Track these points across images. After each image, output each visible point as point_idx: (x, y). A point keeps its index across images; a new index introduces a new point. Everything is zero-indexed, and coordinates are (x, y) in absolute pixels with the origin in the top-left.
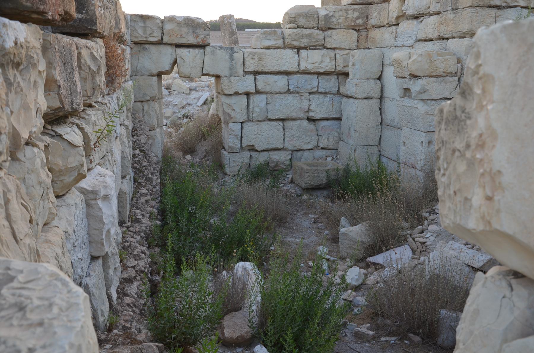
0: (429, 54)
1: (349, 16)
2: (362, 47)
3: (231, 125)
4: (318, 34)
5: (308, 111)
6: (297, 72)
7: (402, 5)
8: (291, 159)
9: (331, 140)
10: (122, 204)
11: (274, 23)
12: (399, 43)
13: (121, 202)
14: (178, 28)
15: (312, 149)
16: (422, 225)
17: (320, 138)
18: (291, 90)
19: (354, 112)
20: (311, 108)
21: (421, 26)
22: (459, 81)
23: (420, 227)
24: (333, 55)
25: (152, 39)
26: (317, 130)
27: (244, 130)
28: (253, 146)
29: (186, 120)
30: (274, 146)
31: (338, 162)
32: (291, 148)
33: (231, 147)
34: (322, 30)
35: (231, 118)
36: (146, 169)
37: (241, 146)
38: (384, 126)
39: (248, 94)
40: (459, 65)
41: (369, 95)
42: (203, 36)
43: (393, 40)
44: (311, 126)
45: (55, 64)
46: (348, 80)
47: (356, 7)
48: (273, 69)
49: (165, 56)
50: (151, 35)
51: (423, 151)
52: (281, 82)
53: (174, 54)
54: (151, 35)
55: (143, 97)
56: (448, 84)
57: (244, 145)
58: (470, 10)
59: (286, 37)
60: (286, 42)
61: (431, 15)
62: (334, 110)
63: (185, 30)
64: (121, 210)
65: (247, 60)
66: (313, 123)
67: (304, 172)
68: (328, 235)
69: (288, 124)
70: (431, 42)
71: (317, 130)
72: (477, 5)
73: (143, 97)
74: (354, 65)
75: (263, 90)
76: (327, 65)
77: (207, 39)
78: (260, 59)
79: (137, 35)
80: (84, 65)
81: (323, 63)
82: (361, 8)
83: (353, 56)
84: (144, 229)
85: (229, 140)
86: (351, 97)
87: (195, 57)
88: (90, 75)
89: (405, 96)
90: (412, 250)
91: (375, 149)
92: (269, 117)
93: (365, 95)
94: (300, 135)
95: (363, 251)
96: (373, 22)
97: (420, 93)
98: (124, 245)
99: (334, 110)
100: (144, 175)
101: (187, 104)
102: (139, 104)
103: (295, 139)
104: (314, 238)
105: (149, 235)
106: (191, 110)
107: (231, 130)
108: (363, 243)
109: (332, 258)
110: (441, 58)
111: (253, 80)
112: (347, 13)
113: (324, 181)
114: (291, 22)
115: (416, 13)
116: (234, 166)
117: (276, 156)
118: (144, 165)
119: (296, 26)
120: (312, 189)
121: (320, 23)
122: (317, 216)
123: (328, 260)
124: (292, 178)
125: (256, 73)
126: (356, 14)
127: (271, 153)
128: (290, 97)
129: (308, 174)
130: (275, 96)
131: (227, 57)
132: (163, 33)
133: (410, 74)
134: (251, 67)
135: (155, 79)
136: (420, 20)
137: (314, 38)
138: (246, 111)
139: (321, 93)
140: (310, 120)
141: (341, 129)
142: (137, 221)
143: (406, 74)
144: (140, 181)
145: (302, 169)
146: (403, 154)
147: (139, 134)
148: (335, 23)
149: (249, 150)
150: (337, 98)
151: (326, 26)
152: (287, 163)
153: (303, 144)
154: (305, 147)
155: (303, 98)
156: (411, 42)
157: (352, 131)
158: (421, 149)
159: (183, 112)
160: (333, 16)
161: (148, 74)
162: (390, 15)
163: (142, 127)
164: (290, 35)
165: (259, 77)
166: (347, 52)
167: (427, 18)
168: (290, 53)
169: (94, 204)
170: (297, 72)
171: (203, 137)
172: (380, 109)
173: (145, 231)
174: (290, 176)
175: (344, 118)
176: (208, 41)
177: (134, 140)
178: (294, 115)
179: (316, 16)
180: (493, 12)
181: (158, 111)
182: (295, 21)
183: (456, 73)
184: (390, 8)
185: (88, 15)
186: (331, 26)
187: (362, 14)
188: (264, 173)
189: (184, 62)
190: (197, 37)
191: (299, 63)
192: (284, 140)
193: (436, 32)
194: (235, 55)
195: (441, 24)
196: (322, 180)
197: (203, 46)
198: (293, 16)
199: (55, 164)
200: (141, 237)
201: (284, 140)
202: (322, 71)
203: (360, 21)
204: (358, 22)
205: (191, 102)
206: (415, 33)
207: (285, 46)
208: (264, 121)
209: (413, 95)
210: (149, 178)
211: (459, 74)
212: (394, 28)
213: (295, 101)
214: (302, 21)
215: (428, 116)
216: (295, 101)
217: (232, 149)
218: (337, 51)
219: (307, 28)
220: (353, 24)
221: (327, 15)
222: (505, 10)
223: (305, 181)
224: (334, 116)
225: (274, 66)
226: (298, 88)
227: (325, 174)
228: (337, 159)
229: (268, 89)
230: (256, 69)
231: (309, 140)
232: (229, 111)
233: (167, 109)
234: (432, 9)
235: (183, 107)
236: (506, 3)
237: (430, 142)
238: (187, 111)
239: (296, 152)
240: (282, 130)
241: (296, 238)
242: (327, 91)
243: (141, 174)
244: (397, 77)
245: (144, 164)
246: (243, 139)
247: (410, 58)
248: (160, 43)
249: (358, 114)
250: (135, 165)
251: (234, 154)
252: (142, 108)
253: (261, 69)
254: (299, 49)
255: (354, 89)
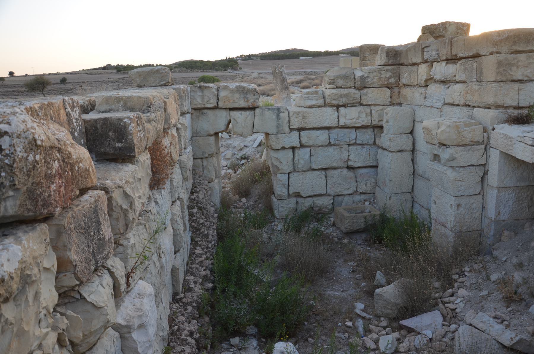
0: (457, 126)
1: (382, 76)
2: (395, 102)
3: (279, 176)
4: (354, 94)
5: (347, 161)
6: (337, 127)
7: (430, 70)
8: (333, 203)
9: (368, 185)
10: (175, 278)
11: (323, 51)
12: (428, 103)
13: (174, 276)
14: (231, 95)
15: (352, 194)
16: (452, 288)
17: (358, 183)
18: (332, 143)
19: (389, 163)
20: (350, 158)
21: (448, 91)
22: (485, 149)
23: (450, 290)
24: (369, 111)
25: (209, 106)
26: (356, 177)
27: (290, 180)
28: (299, 193)
29: (243, 161)
30: (317, 193)
31: (375, 206)
32: (332, 193)
33: (280, 195)
34: (358, 89)
35: (279, 170)
36: (203, 226)
37: (288, 193)
38: (416, 175)
39: (293, 148)
40: (486, 134)
41: (402, 148)
42: (252, 100)
43: (423, 100)
44: (351, 174)
45: (69, 246)
46: (383, 134)
47: (389, 67)
48: (315, 126)
49: (222, 117)
50: (208, 102)
51: (453, 213)
52: (322, 137)
53: (228, 116)
54: (208, 102)
55: (203, 155)
56: (475, 152)
57: (291, 193)
58: (494, 84)
59: (327, 97)
60: (327, 101)
61: (458, 82)
62: (371, 159)
63: (237, 95)
64: (174, 283)
65: (292, 118)
66: (352, 170)
67: (345, 218)
68: (364, 286)
69: (330, 173)
70: (458, 107)
71: (356, 177)
72: (500, 80)
73: (203, 155)
74: (387, 122)
75: (307, 144)
76: (364, 120)
77: (257, 102)
78: (304, 117)
79: (196, 103)
80: (115, 207)
81: (360, 119)
82: (393, 69)
83: (387, 114)
84: (195, 298)
85: (278, 189)
86: (386, 149)
87: (247, 118)
88: (122, 214)
89: (434, 160)
90: (443, 315)
91: (409, 196)
92: (313, 168)
93: (398, 149)
94: (341, 183)
95: (396, 312)
96: (404, 81)
97: (448, 160)
98: (173, 330)
99: (371, 159)
100: (201, 233)
101: (245, 146)
102: (199, 160)
103: (336, 186)
104: (351, 291)
105: (200, 304)
106: (247, 152)
107: (279, 180)
108: (396, 304)
109: (368, 316)
110: (467, 128)
111: (298, 135)
112: (380, 73)
113: (363, 226)
114: (330, 84)
115: (443, 79)
116: (282, 211)
117: (320, 202)
118: (201, 222)
119: (335, 87)
120: (350, 234)
121: (356, 83)
122: (355, 264)
123: (364, 318)
124: (334, 222)
125: (300, 130)
126: (389, 74)
127: (315, 199)
128: (331, 150)
129: (348, 221)
130: (317, 148)
131: (274, 117)
132: (218, 99)
133: (439, 143)
134: (296, 124)
135: (212, 138)
136: (447, 86)
137: (351, 97)
138: (292, 163)
139: (359, 144)
140: (349, 168)
141: (377, 175)
142: (190, 290)
143: (436, 142)
144: (196, 239)
145: (343, 215)
146: (434, 212)
147: (198, 190)
148: (370, 83)
149: (296, 196)
150: (374, 149)
151: (362, 85)
152: (330, 207)
153: (343, 189)
154: (346, 192)
155: (343, 150)
156: (439, 104)
157: (388, 181)
158: (451, 211)
159: (241, 153)
160: (368, 77)
161: (206, 134)
162: (420, 77)
163: (202, 182)
164: (329, 95)
165: (303, 133)
166: (381, 107)
167: (453, 85)
168: (330, 111)
169: (129, 337)
170: (337, 127)
171: (255, 182)
172: (412, 160)
173: (196, 300)
174: (332, 219)
175: (380, 166)
176: (258, 104)
177: (193, 197)
178: (335, 165)
179: (352, 77)
180: (516, 86)
181: (216, 165)
182: (334, 83)
183: (483, 141)
184: (419, 72)
185: (127, 143)
186: (366, 86)
187: (394, 73)
188: (307, 218)
189: (237, 123)
190: (248, 101)
191: (338, 119)
192: (326, 187)
193: (462, 99)
194: (282, 115)
195: (467, 93)
196: (361, 225)
197: (253, 109)
198: (332, 78)
199: (76, 337)
200: (193, 307)
201: (326, 187)
202: (359, 125)
203: (392, 80)
204: (390, 81)
205: (248, 144)
206: (442, 96)
207: (325, 105)
208: (308, 170)
209: (443, 162)
210: (205, 234)
211: (485, 142)
212: (423, 89)
213: (336, 153)
214: (340, 82)
215: (457, 182)
216: (336, 153)
217: (281, 197)
218: (372, 107)
219: (345, 88)
220: (386, 83)
221: (363, 76)
222: (527, 84)
223: (346, 226)
224: (371, 165)
225: (316, 123)
226: (338, 141)
227: (363, 220)
228: (374, 203)
229: (311, 143)
230: (300, 126)
231: (348, 187)
232: (277, 164)
233: (228, 151)
234: (458, 78)
235: (241, 149)
236: (528, 77)
237: (459, 205)
238: (244, 153)
239: (337, 197)
240: (324, 178)
241: (336, 291)
242: (364, 142)
243: (198, 232)
244: (427, 142)
245: (201, 221)
246: (290, 188)
247: (439, 127)
248: (216, 108)
249: (392, 165)
250: (193, 224)
251: (282, 201)
252: (201, 164)
253: (304, 125)
254: (338, 107)
255: (388, 143)
